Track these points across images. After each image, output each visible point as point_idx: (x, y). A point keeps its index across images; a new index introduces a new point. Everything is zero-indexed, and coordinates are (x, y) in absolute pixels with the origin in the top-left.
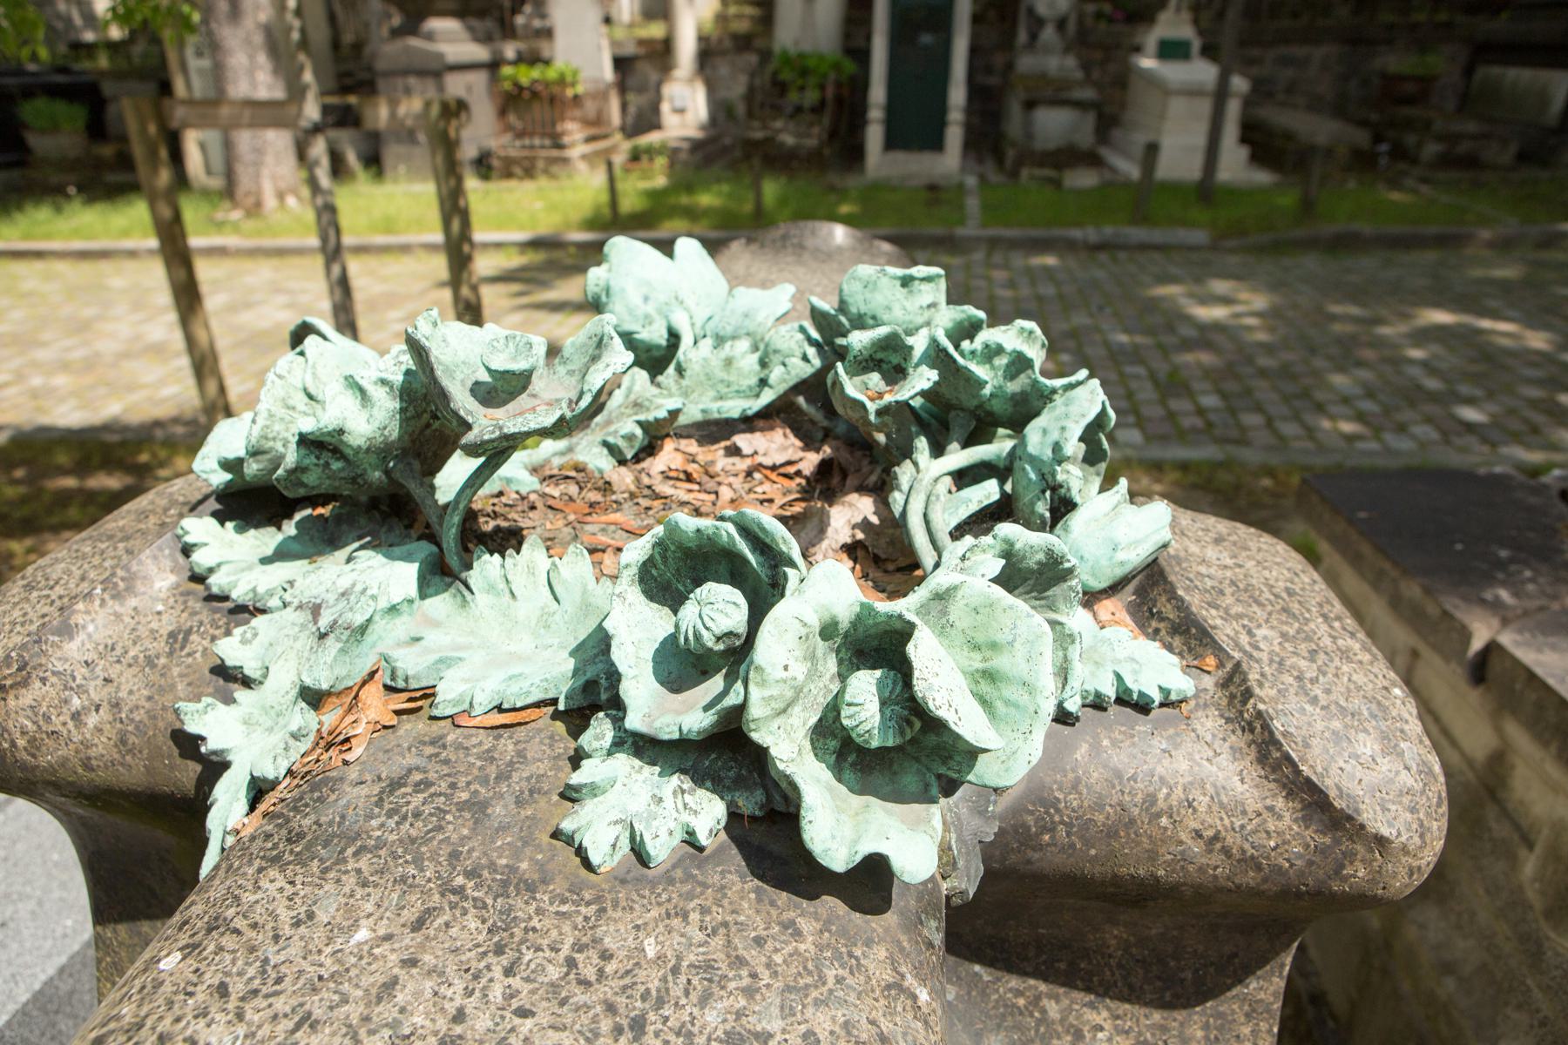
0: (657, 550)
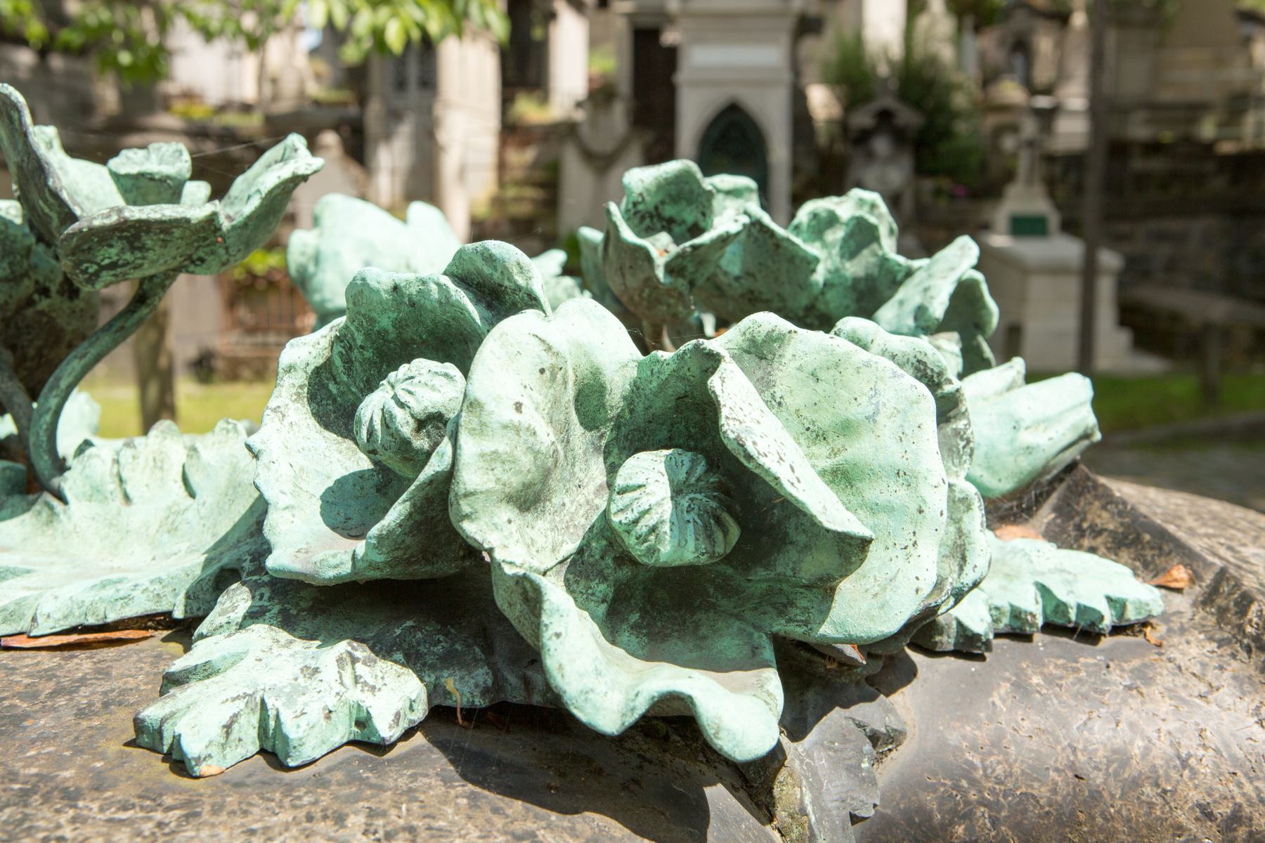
0: (338, 348)
